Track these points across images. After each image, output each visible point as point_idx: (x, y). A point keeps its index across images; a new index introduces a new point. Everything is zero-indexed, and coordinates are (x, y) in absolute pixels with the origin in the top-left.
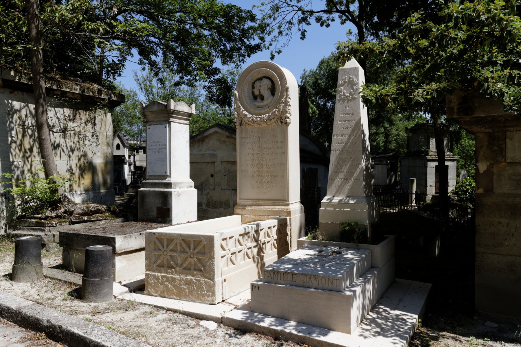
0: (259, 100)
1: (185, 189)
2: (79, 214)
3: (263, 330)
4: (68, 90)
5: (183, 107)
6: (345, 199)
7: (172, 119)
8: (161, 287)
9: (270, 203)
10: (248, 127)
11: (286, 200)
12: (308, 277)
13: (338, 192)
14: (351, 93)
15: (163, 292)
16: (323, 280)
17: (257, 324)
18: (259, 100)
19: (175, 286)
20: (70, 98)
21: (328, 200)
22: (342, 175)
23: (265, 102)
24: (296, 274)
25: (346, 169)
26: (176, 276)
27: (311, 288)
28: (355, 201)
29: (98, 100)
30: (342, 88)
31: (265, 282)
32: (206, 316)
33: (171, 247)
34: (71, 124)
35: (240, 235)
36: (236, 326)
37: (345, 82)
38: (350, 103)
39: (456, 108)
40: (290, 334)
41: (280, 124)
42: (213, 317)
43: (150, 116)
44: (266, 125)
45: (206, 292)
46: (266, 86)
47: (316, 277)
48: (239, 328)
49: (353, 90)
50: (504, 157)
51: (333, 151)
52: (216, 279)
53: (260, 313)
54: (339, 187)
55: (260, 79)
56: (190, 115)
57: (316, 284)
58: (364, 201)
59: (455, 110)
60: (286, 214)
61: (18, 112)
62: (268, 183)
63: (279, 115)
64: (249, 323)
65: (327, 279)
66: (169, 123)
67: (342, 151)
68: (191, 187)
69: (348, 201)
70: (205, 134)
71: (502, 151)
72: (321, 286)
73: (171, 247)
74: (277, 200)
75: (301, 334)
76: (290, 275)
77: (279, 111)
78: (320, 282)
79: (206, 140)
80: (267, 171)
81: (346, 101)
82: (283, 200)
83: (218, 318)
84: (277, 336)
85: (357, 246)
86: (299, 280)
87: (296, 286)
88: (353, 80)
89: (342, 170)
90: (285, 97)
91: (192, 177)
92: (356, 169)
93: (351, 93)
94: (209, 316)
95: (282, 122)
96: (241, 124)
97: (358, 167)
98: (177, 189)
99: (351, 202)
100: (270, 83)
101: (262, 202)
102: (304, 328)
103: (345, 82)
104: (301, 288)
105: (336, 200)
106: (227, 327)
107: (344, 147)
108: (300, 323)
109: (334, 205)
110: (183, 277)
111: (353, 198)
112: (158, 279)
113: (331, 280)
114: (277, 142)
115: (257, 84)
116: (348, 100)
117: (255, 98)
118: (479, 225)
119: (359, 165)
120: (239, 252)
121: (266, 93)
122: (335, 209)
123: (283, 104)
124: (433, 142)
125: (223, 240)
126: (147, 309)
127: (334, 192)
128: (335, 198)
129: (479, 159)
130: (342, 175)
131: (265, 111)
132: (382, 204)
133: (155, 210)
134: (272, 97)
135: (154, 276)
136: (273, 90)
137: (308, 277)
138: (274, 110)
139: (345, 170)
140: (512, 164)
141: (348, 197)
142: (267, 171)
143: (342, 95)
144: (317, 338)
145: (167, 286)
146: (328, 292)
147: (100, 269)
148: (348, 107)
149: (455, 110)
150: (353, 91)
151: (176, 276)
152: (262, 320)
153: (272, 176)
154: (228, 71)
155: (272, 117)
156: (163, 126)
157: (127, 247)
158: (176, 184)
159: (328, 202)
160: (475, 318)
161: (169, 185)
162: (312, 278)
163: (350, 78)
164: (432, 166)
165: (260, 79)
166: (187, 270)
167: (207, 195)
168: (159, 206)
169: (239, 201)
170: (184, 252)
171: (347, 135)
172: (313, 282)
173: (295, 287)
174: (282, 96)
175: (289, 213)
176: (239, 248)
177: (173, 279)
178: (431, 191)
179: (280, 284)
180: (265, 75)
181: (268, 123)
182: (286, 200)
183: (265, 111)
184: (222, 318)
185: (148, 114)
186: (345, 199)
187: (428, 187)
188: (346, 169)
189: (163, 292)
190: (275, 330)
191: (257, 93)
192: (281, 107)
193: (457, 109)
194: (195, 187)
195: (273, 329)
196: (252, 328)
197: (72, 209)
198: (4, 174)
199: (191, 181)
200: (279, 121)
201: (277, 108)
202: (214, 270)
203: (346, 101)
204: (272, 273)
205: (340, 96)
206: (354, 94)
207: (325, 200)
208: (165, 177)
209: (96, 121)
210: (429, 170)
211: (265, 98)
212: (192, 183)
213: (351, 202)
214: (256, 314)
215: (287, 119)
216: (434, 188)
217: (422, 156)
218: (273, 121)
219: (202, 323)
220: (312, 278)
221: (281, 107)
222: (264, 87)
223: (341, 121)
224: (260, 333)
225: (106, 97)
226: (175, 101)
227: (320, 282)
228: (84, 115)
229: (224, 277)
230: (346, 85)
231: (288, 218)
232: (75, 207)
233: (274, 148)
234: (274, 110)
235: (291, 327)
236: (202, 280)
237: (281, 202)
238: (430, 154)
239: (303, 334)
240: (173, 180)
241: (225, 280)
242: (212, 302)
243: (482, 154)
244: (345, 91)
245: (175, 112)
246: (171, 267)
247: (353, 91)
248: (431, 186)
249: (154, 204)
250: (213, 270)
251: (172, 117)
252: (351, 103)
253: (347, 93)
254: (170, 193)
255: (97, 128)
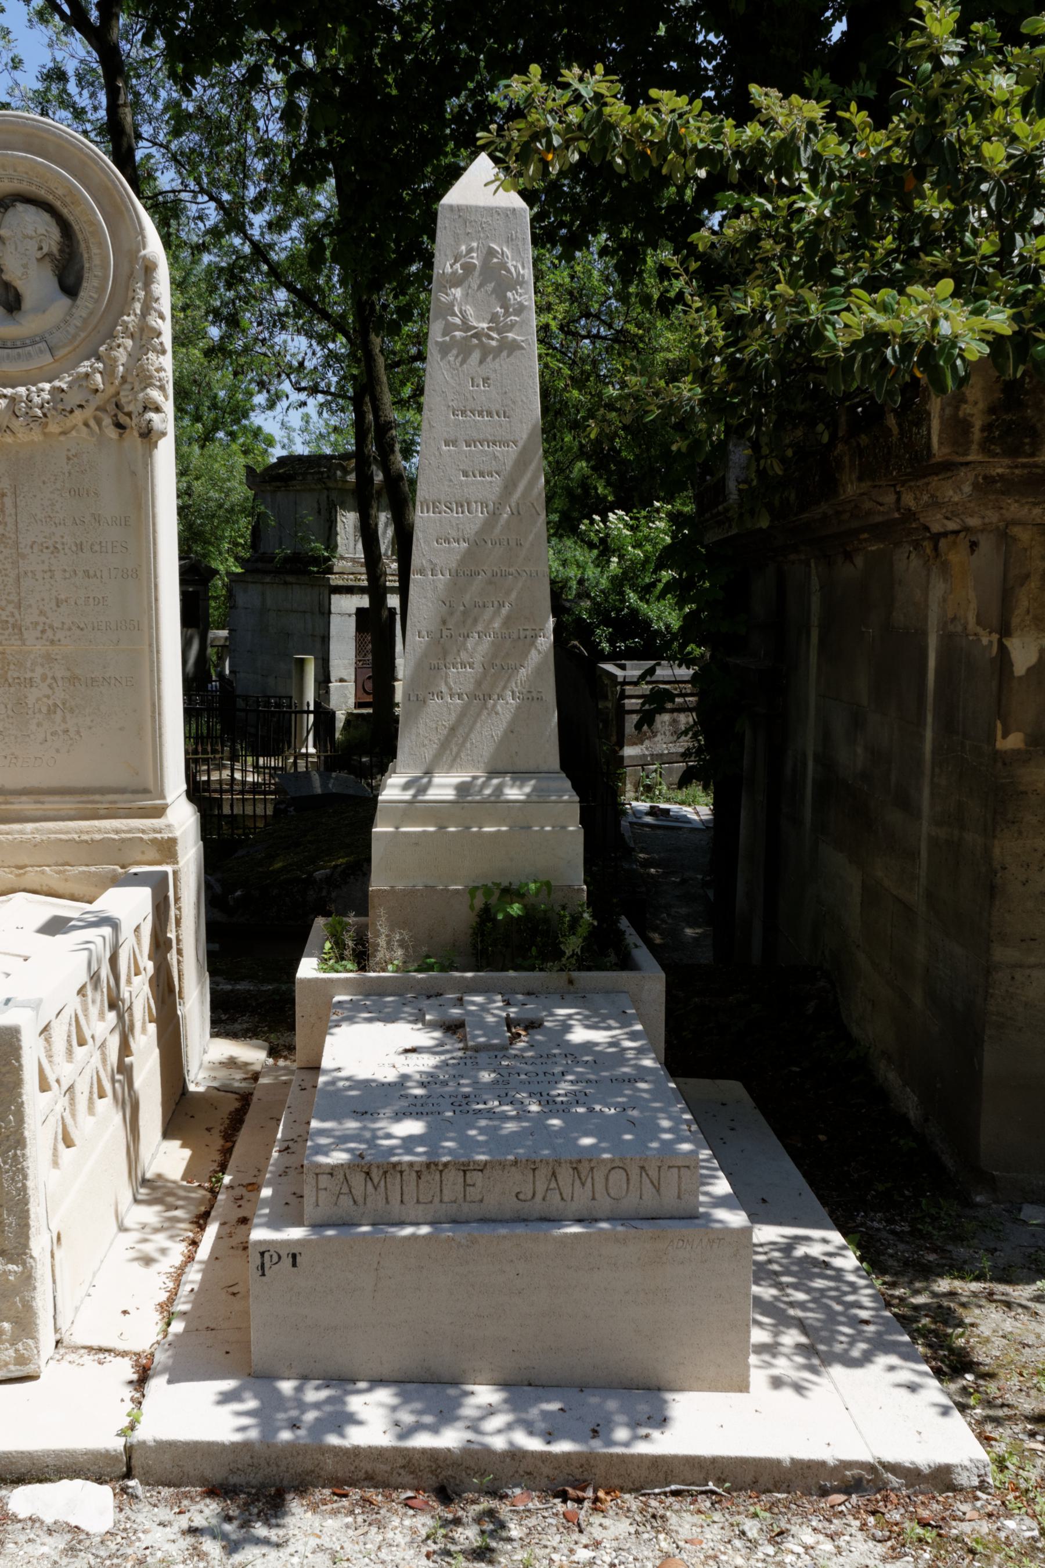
3: (367, 1466)
6: (484, 785)
9: (68, 804)
11: (146, 791)
12: (543, 1172)
13: (448, 750)
14: (494, 318)
16: (617, 1176)
17: (333, 1440)
21: (406, 787)
22: (460, 677)
23: (28, 325)
24: (482, 1168)
25: (478, 648)
27: (557, 1220)
28: (527, 789)
30: (458, 292)
31: (317, 1226)
32: (29, 1456)
36: (217, 1474)
37: (468, 268)
38: (492, 365)
39: (978, 424)
40: (515, 1454)
41: (112, 433)
42: (72, 1454)
44: (36, 436)
46: (32, 246)
47: (584, 1168)
48: (234, 1480)
49: (505, 306)
51: (421, 572)
53: (305, 1378)
54: (453, 729)
57: (580, 1199)
58: (561, 792)
59: (977, 434)
60: (152, 854)
61: (629, 108)
62: (52, 710)
63: (111, 390)
64: (290, 1444)
65: (634, 1172)
67: (464, 572)
69: (499, 790)
72: (604, 1204)
74: (103, 791)
75: (563, 1447)
76: (453, 1177)
77: (108, 373)
78: (600, 1186)
80: (49, 658)
81: (476, 355)
82: (135, 792)
83: (106, 1456)
84: (442, 1481)
85: (571, 982)
86: (497, 1193)
87: (483, 1220)
88: (503, 266)
89: (464, 655)
90: (138, 307)
92: (525, 654)
93: (494, 318)
94: (47, 1453)
95: (119, 426)
97: (533, 644)
99: (514, 793)
100: (55, 233)
101: (24, 804)
102: (553, 1406)
103: (468, 268)
104: (520, 1230)
105: (443, 788)
106: (166, 1492)
107: (469, 556)
108: (521, 1387)
109: (437, 812)
111: (519, 775)
113: (653, 1173)
114: (97, 519)
116: (486, 352)
118: (1004, 868)
119: (535, 637)
121: (35, 283)
122: (442, 827)
123: (129, 343)
124: (348, 521)
127: (429, 754)
128: (437, 780)
129: (1015, 621)
130: (460, 677)
131: (33, 365)
132: (205, 752)
134: (65, 301)
137: (543, 1172)
138: (85, 367)
139: (478, 658)
141: (492, 773)
142: (49, 658)
143: (456, 327)
144: (642, 1448)
146: (647, 1229)
148: (486, 380)
149: (977, 434)
150: (507, 313)
152: (343, 1420)
153: (73, 679)
155: (74, 398)
159: (407, 795)
160: (978, 1199)
162: (565, 1174)
163: (491, 253)
164: (345, 608)
171: (484, 504)
172: (567, 1192)
173: (486, 1229)
174: (121, 303)
178: (344, 699)
179: (402, 1224)
180: (23, 187)
181: (53, 428)
182: (146, 791)
183: (33, 365)
184: (129, 1449)
186: (484, 785)
187: (333, 686)
188: (478, 648)
190: (432, 1455)
192: (121, 356)
193: (982, 430)
195: (424, 1451)
196: (309, 1465)
200: (107, 421)
201: (99, 359)
202: (25, 1201)
203: (476, 355)
204: (358, 1180)
205: (448, 329)
206: (511, 327)
207: (393, 789)
210: (335, 622)
211: (27, 303)
213: (514, 793)
214: (287, 1387)
215: (152, 415)
216: (351, 686)
217: (309, 570)
218: (79, 416)
220: (565, 1174)
221: (121, 356)
223: (454, 443)
224: (353, 1484)
227: (600, 1186)
230: (474, 281)
233: (80, 547)
234: (85, 367)
235: (488, 1420)
237: (123, 801)
238: (339, 565)
239: (574, 1439)
242: (16, 1371)
243: (1024, 603)
244: (470, 310)
247: (507, 313)
248: (342, 680)
252: (496, 365)
253: (479, 319)
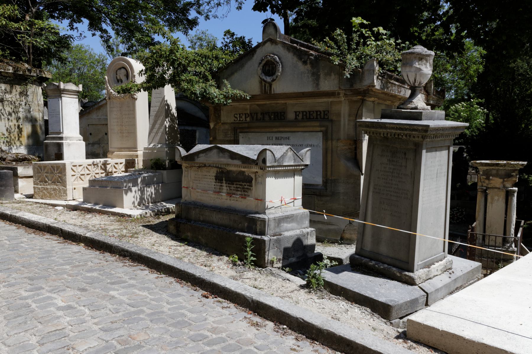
0: (120, 82)
1: (76, 142)
2: (10, 160)
4: (3, 70)
5: (71, 87)
7: (62, 95)
8: (41, 193)
9: (127, 150)
10: (114, 101)
15: (42, 196)
18: (120, 82)
19: (48, 192)
20: (5, 76)
26: (48, 187)
29: (28, 77)
33: (46, 171)
34: (8, 96)
35: (88, 165)
43: (49, 93)
45: (62, 194)
50: (220, 120)
52: (68, 187)
55: (120, 69)
56: (78, 92)
66: (61, 97)
68: (80, 140)
70: (100, 104)
71: (219, 116)
73: (46, 171)
79: (102, 109)
91: (81, 134)
96: (109, 99)
98: (68, 141)
101: (123, 150)
110: (52, 187)
112: (39, 189)
115: (118, 72)
117: (118, 81)
120: (87, 174)
121: (124, 78)
125: (74, 166)
126: (30, 203)
133: (54, 155)
135: (38, 188)
136: (127, 76)
140: (223, 124)
145: (44, 193)
147: (5, 183)
151: (48, 187)
153: (128, 133)
154: (196, 36)
156: (57, 99)
157: (26, 173)
158: (67, 138)
161: (61, 138)
165: (120, 69)
166: (54, 182)
167: (103, 148)
168: (56, 152)
169: (110, 149)
170: (52, 173)
175: (137, 156)
176: (88, 172)
177: (47, 189)
185: (48, 91)
189: (42, 196)
191: (118, 78)
194: (84, 140)
197: (5, 157)
198: (272, 255)
199: (80, 136)
208: (60, 133)
209: (28, 93)
212: (82, 138)
219: (56, 208)
222: (122, 74)
225: (35, 75)
226: (64, 82)
228: (18, 89)
229: (74, 187)
231: (136, 159)
232: (7, 155)
236: (61, 187)
240: (64, 135)
241: (75, 189)
245: (64, 90)
246: (46, 182)
249: (53, 151)
250: (66, 182)
251: (63, 93)
254: (62, 143)
255: (30, 98)
